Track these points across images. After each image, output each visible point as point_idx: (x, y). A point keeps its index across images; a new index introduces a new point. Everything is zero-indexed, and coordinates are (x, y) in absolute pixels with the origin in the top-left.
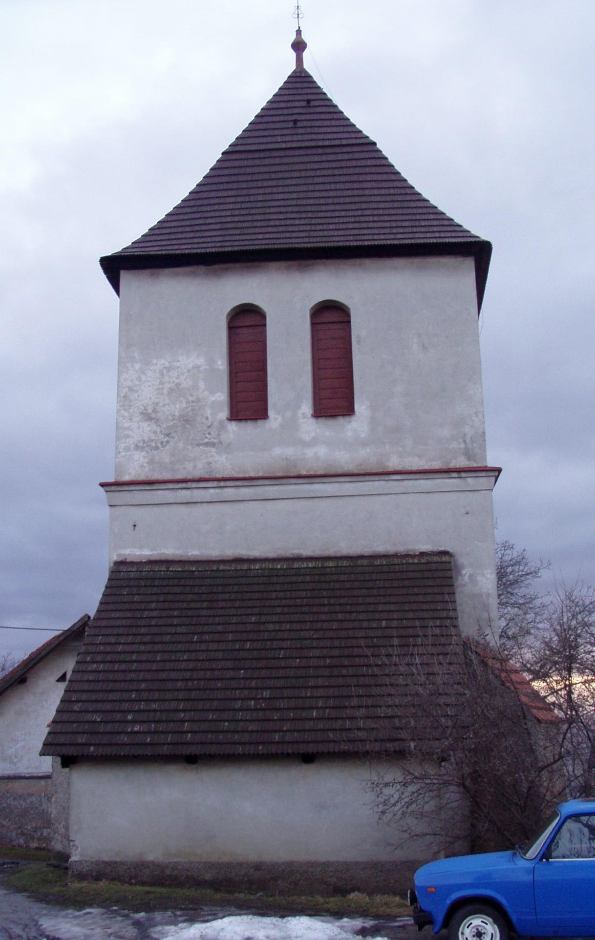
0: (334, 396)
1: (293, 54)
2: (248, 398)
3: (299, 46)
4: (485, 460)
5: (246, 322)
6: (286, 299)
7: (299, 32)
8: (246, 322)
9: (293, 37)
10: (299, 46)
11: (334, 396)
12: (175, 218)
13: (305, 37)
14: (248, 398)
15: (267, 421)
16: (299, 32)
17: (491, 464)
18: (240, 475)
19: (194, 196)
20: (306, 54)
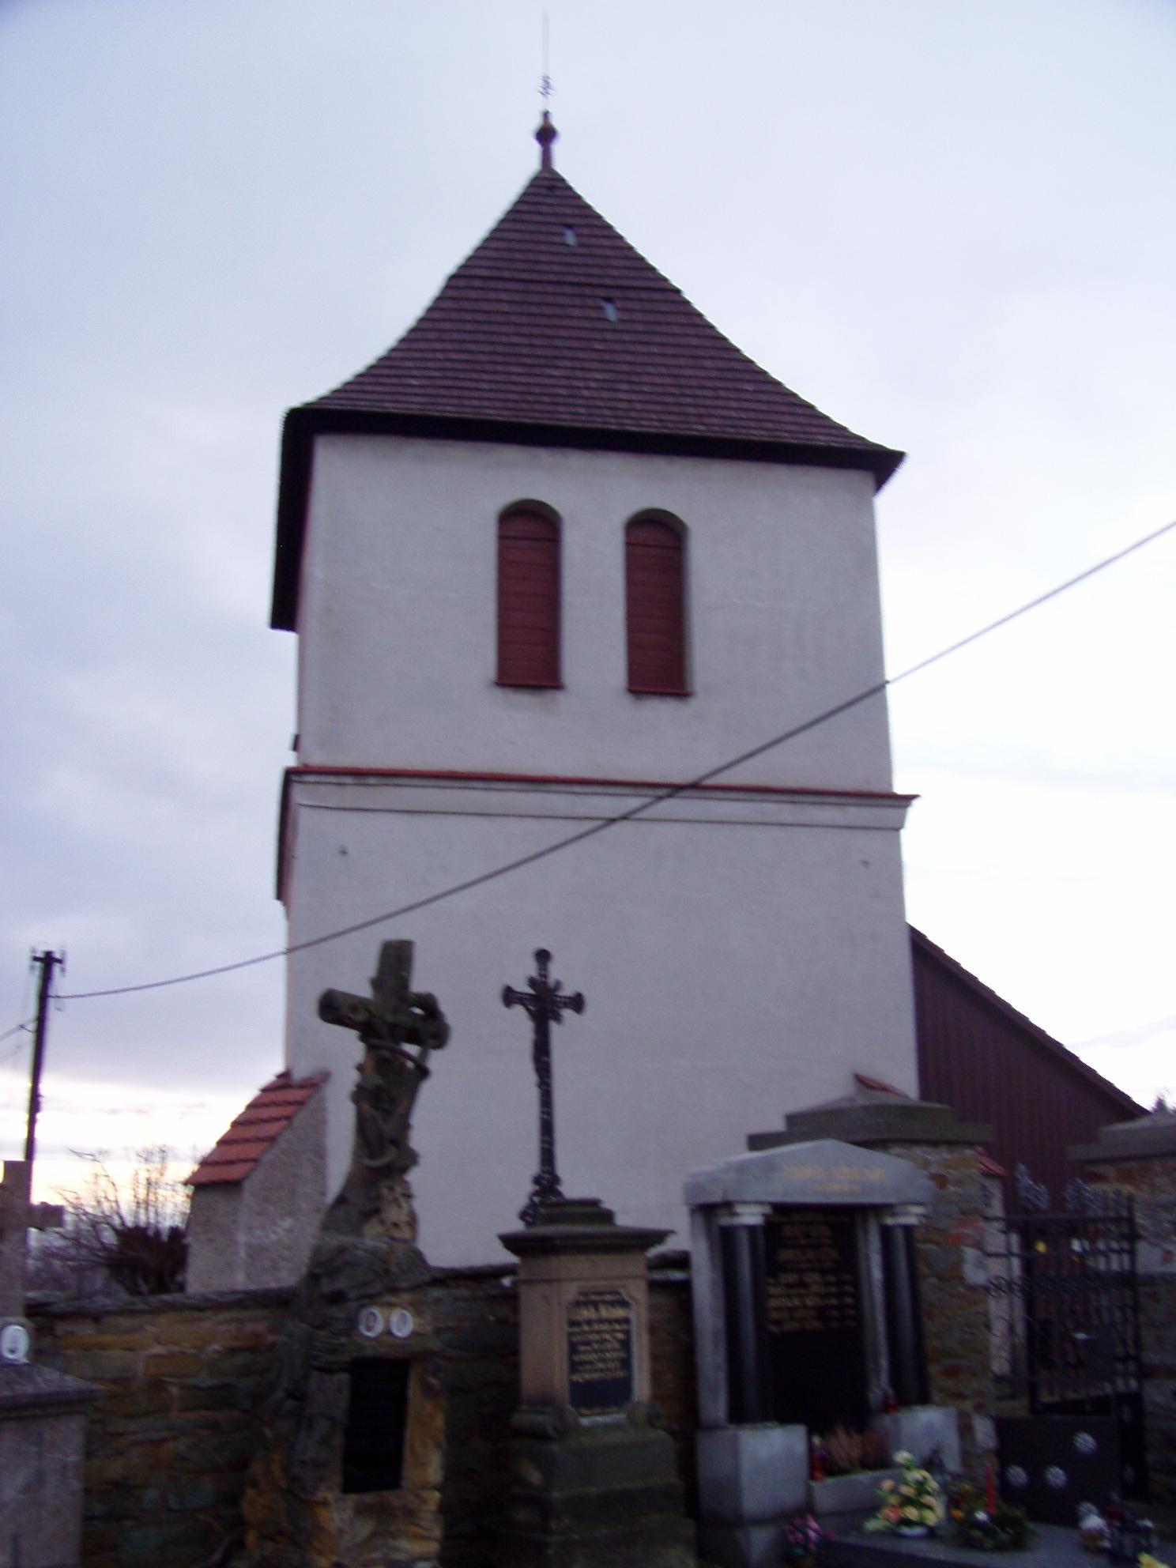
0: (659, 663)
1: (536, 148)
2: (529, 657)
3: (546, 135)
4: (890, 785)
5: (530, 534)
6: (595, 502)
7: (546, 115)
8: (530, 534)
9: (536, 122)
10: (546, 135)
11: (659, 663)
12: (357, 388)
13: (555, 122)
14: (529, 657)
15: (560, 696)
16: (546, 115)
17: (899, 789)
18: (816, 830)
19: (405, 346)
20: (558, 148)
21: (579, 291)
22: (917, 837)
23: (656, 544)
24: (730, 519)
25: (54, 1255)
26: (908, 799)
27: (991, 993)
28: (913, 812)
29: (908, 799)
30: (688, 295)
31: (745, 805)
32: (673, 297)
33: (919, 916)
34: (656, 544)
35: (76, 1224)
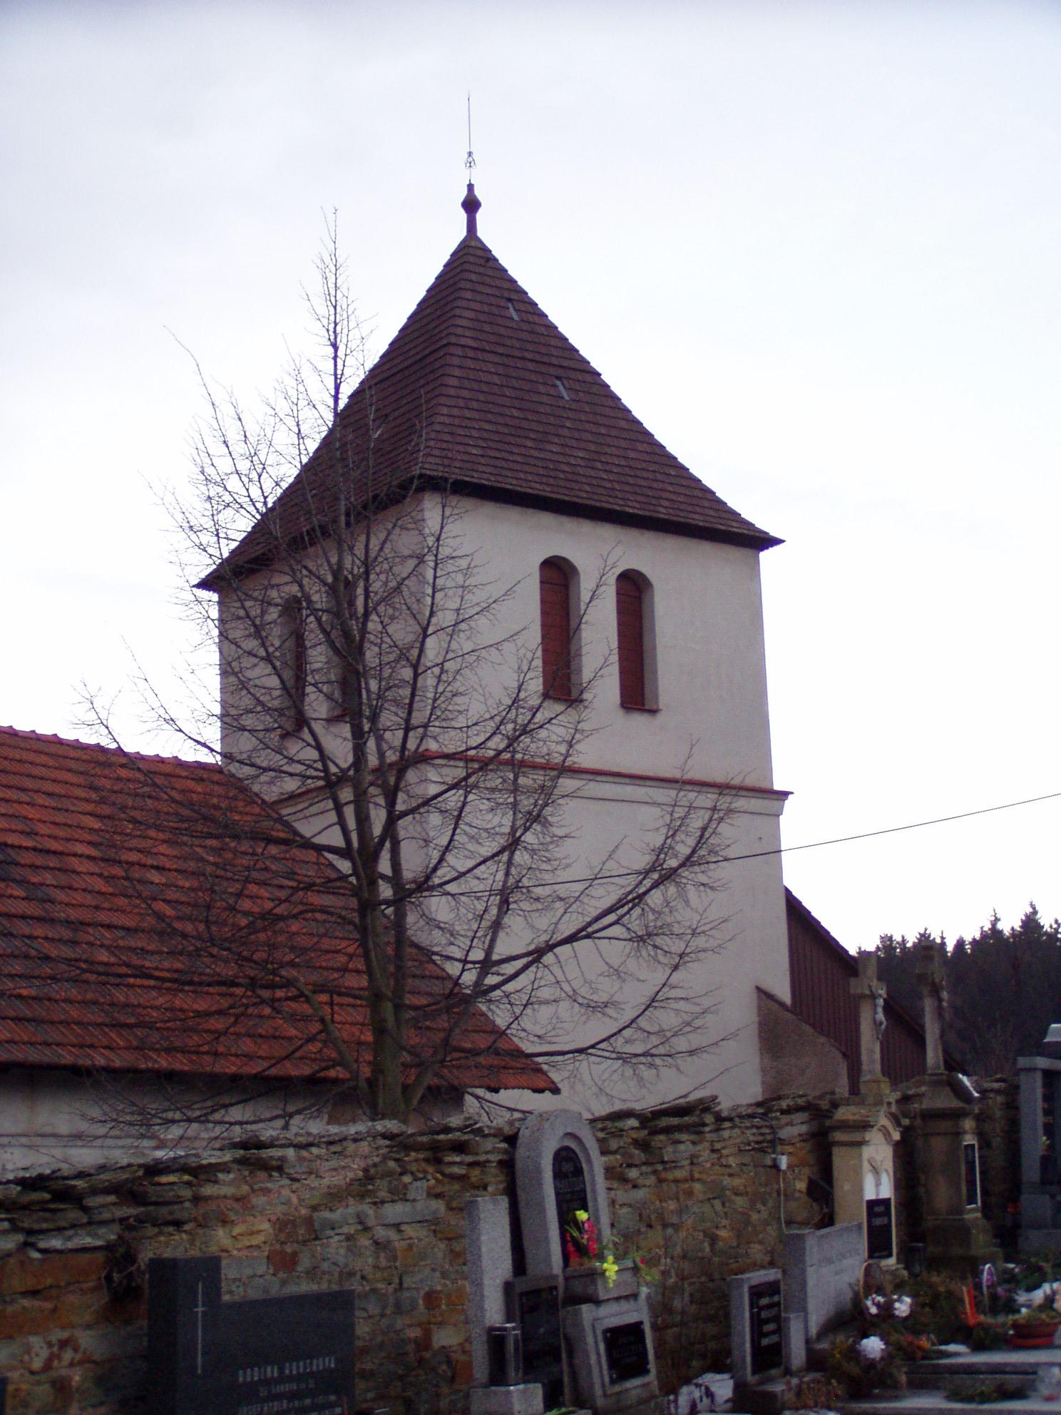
1: (463, 216)
3: (471, 205)
5: (558, 576)
7: (470, 187)
8: (558, 576)
10: (471, 205)
11: (636, 694)
13: (478, 193)
16: (470, 187)
17: (778, 786)
21: (506, 361)
22: (793, 825)
23: (633, 590)
24: (672, 568)
25: (449, 1362)
26: (785, 795)
27: (828, 933)
28: (789, 803)
29: (785, 795)
30: (605, 377)
31: (761, 801)
32: (588, 378)
33: (788, 882)
34: (633, 590)
35: (995, 1245)
